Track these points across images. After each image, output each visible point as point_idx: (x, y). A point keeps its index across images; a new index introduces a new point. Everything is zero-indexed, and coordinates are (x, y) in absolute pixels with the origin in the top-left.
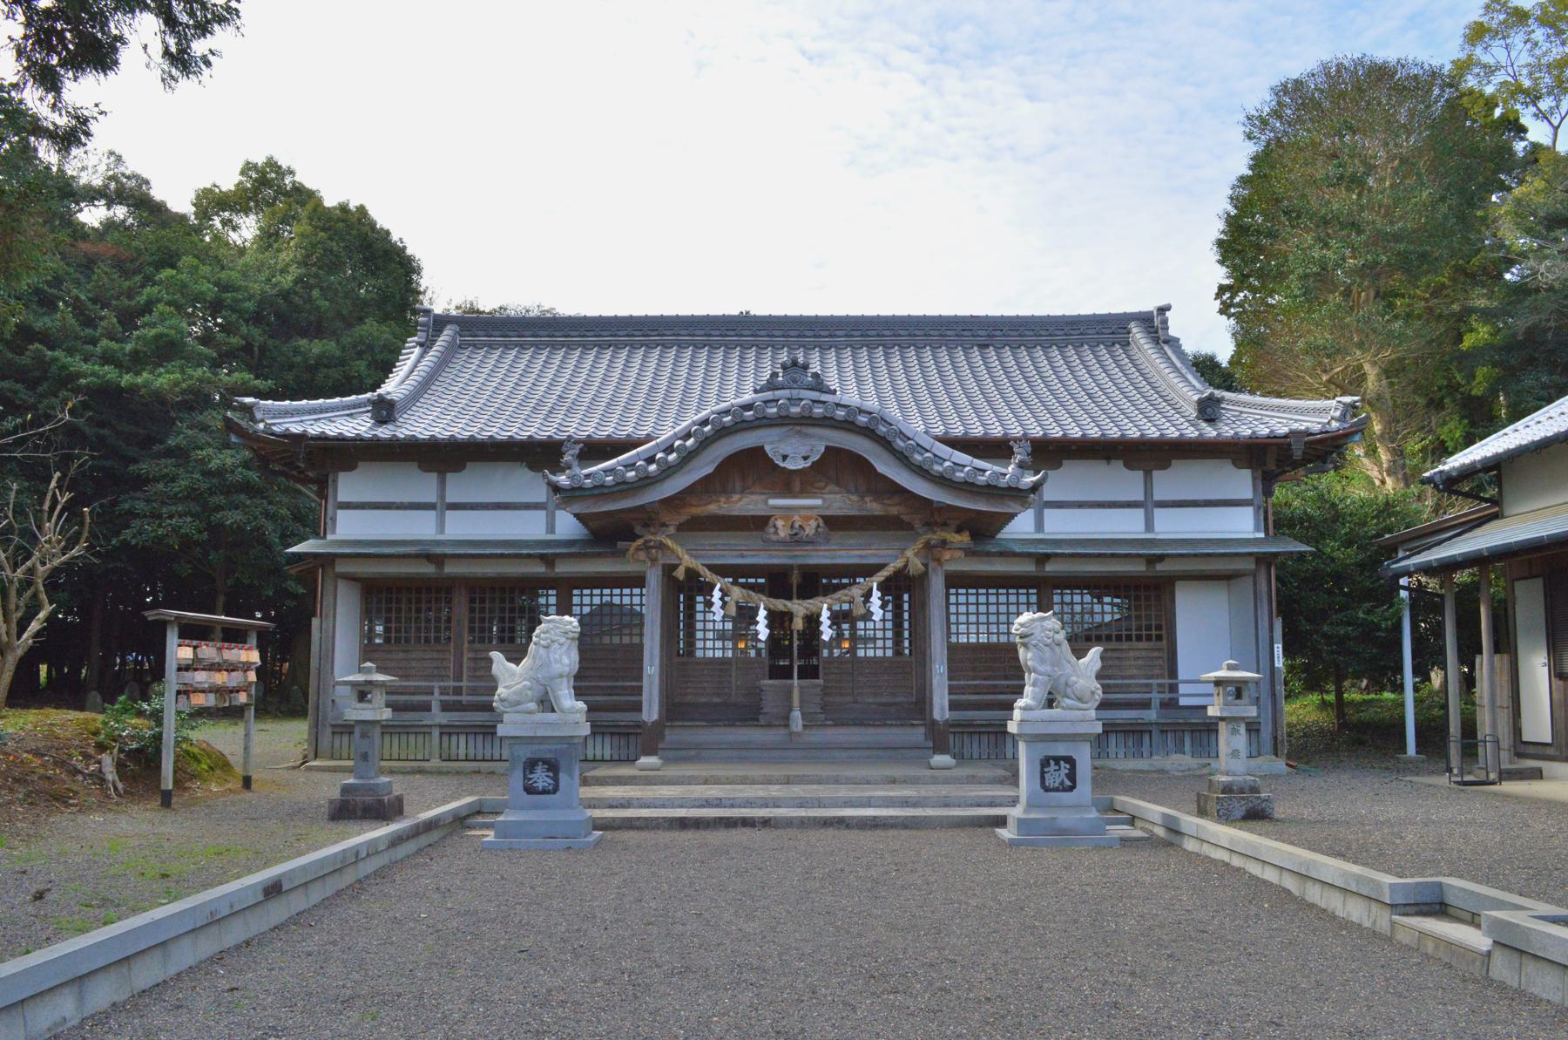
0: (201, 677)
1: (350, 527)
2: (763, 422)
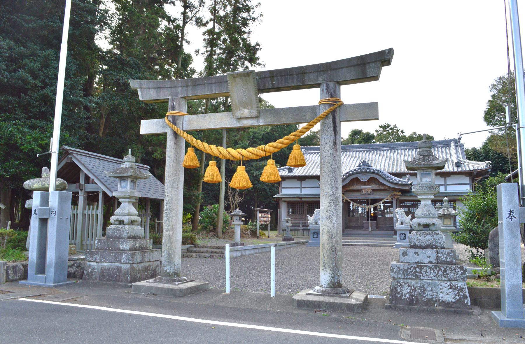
0: (262, 219)
1: (285, 192)
2: (358, 173)
